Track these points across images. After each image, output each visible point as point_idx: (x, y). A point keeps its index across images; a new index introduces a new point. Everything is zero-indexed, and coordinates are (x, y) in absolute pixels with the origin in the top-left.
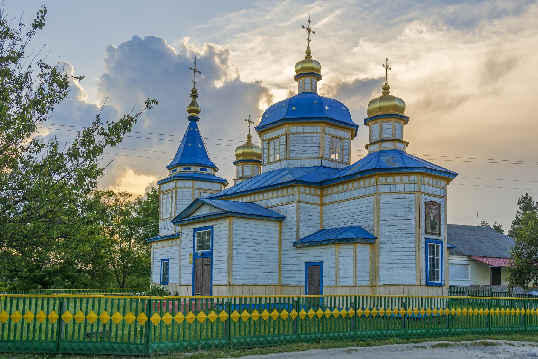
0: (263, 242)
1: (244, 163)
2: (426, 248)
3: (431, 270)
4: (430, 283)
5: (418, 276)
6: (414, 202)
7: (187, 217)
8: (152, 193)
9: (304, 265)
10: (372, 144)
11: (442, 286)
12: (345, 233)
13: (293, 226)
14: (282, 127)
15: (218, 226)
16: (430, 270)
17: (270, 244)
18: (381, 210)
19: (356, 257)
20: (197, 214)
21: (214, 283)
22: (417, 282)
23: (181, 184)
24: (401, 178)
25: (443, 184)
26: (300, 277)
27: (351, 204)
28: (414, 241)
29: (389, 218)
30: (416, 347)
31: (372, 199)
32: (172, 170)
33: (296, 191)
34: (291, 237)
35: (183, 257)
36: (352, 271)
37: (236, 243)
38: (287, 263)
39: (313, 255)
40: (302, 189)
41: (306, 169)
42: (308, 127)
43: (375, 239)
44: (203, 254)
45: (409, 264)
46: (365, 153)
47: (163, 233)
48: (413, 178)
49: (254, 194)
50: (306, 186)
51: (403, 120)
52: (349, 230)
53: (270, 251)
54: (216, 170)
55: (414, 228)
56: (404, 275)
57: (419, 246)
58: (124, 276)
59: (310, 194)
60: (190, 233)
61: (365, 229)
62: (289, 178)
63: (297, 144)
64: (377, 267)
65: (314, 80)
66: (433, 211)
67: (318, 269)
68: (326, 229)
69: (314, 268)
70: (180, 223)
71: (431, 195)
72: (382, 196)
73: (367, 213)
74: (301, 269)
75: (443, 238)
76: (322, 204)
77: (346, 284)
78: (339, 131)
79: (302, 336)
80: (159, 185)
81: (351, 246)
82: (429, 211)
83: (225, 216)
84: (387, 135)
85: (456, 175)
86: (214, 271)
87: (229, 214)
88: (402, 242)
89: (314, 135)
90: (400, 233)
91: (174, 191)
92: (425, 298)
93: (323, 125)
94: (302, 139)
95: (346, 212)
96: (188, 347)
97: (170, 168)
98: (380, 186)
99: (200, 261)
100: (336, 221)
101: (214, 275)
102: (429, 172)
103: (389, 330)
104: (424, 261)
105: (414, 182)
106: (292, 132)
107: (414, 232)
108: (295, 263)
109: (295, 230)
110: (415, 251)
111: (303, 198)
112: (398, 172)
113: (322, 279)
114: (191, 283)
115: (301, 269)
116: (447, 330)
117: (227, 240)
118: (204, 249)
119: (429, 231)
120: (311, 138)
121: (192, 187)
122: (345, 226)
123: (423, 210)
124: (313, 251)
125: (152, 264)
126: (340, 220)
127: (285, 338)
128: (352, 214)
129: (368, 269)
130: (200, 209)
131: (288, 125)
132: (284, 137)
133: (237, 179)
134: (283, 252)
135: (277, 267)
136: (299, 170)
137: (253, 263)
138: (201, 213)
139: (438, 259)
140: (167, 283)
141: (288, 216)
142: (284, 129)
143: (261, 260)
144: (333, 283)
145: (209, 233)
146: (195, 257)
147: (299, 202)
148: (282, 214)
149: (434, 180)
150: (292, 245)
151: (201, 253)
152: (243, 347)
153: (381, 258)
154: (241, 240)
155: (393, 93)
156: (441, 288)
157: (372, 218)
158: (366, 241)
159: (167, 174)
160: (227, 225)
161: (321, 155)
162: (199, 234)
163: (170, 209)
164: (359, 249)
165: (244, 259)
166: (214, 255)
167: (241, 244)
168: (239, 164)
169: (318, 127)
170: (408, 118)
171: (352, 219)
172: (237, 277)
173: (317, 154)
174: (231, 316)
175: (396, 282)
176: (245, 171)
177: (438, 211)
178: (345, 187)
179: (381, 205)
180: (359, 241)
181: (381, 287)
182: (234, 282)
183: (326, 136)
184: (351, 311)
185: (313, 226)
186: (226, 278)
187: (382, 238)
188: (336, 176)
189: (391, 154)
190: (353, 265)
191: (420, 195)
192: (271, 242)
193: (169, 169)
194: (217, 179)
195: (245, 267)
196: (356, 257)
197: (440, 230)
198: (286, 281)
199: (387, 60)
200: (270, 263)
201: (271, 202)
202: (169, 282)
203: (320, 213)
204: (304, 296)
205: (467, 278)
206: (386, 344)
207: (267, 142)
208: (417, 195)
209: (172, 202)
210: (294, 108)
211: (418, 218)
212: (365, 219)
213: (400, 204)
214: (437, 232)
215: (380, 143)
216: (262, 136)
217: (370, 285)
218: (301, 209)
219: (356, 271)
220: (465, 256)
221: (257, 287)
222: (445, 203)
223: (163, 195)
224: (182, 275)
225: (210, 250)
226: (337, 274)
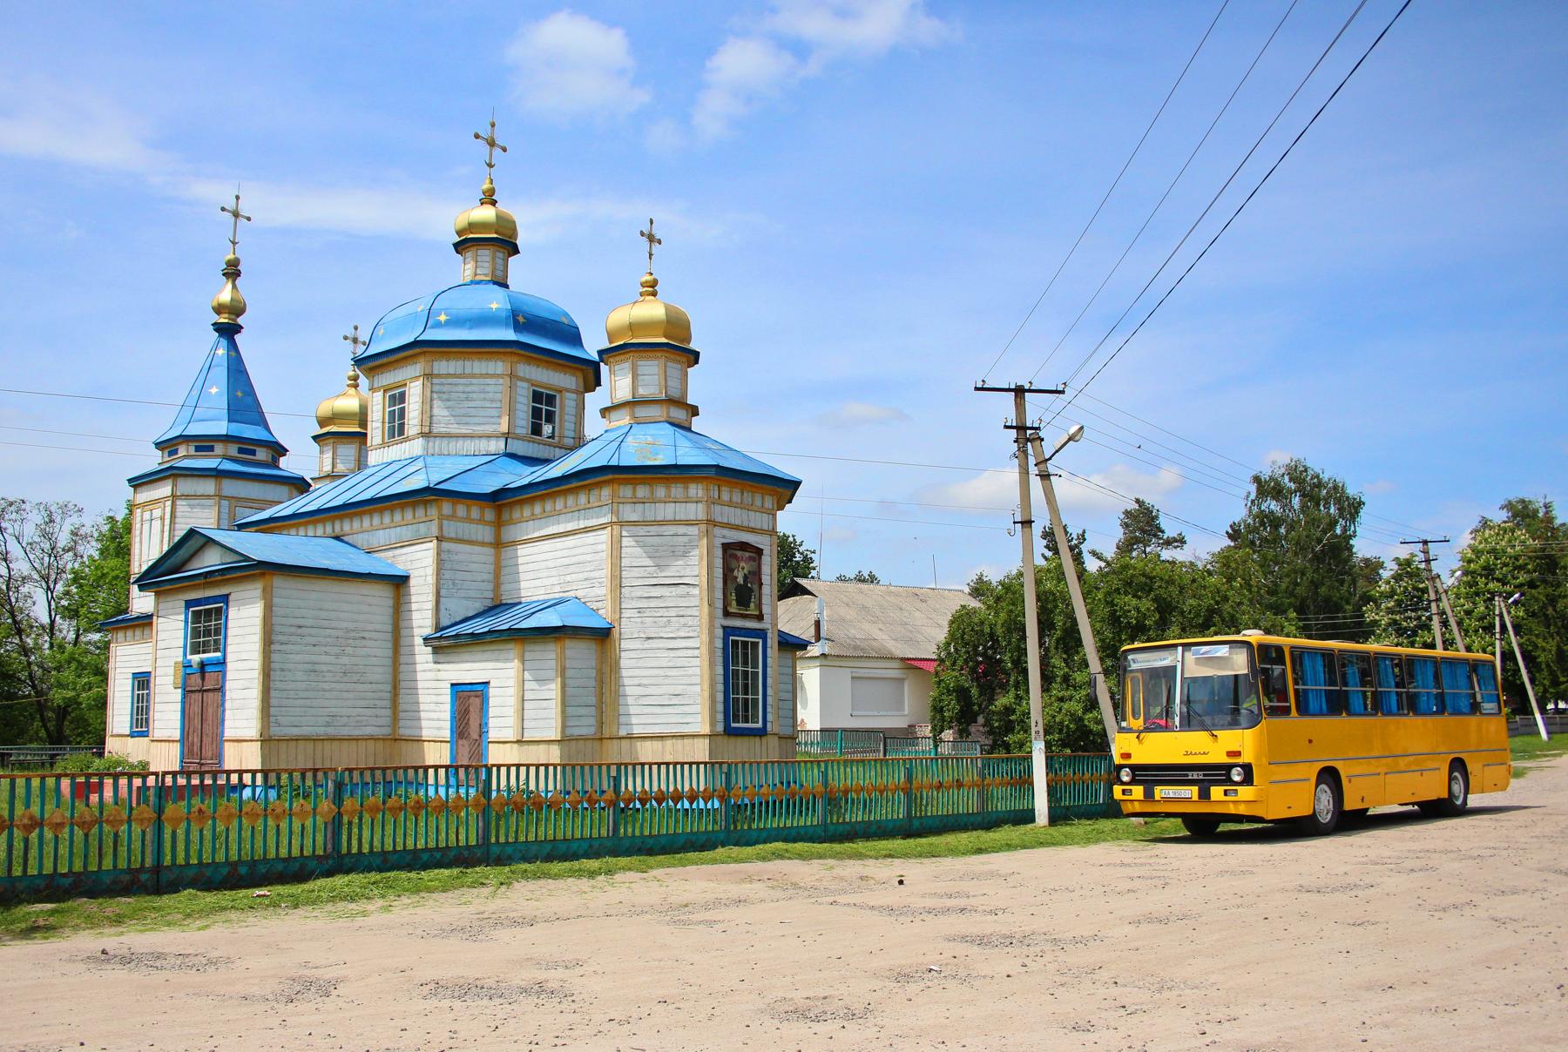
0: (352, 634)
1: (335, 440)
3: (738, 699)
4: (735, 728)
17: (370, 639)
26: (438, 720)
44: (203, 665)
53: (369, 656)
64: (613, 694)
66: (742, 564)
68: (506, 604)
75: (769, 626)
82: (734, 564)
86: (228, 705)
89: (489, 381)
94: (461, 388)
98: (621, 505)
101: (228, 714)
105: (695, 499)
106: (435, 372)
118: (209, 652)
119: (733, 609)
120: (482, 387)
137: (326, 686)
141: (413, 574)
143: (345, 679)
145: (219, 610)
154: (293, 630)
156: (764, 739)
159: (153, 460)
165: (300, 676)
166: (230, 666)
167: (293, 639)
169: (500, 364)
172: (282, 720)
183: (519, 383)
191: (710, 527)
193: (162, 450)
197: (759, 606)
200: (370, 686)
209: (163, 531)
214: (753, 611)
221: (336, 744)
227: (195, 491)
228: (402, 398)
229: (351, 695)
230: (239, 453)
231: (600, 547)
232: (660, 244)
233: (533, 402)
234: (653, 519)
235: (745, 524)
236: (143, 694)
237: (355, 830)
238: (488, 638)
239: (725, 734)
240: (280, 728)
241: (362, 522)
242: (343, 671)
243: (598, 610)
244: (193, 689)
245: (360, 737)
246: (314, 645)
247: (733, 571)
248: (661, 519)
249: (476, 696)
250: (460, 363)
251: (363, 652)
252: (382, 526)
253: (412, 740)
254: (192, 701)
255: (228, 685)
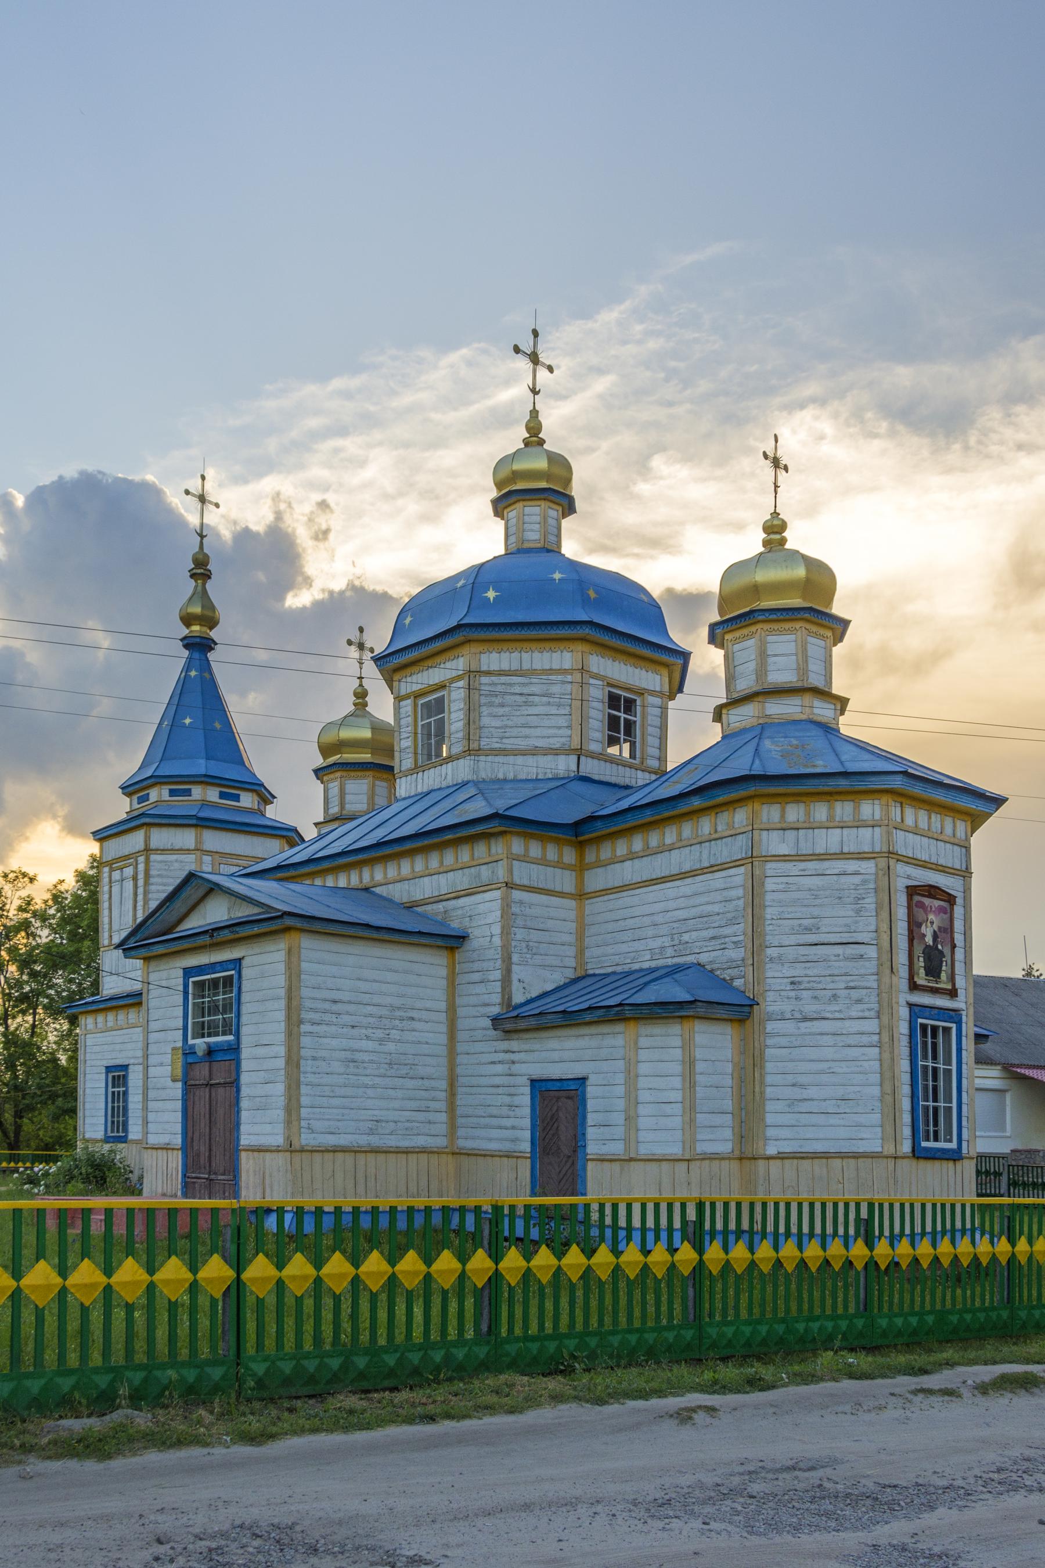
0: (398, 1013)
1: (344, 774)
2: (910, 1036)
4: (926, 1149)
5: (889, 1129)
6: (872, 886)
7: (164, 934)
8: (91, 873)
9: (527, 1090)
10: (734, 702)
11: (961, 1158)
12: (653, 987)
13: (491, 963)
14: (456, 652)
15: (256, 959)
16: (925, 1068)
17: (420, 1020)
18: (769, 910)
19: (690, 1063)
20: (194, 923)
21: (244, 1141)
22: (886, 1148)
23: (160, 837)
24: (831, 809)
25: (961, 832)
26: (513, 1128)
27: (671, 893)
28: (873, 1014)
29: (793, 939)
30: (922, 1391)
31: (739, 875)
32: (135, 797)
33: (500, 851)
34: (486, 998)
35: (152, 1060)
36: (677, 1109)
37: (311, 1015)
38: (474, 1081)
39: (555, 1055)
40: (517, 845)
41: (530, 785)
42: (536, 655)
43: (751, 1006)
45: (858, 1088)
46: (714, 734)
47: (111, 986)
48: (870, 809)
49: (371, 862)
50: (532, 836)
51: (832, 629)
52: (667, 975)
53: (419, 1042)
54: (266, 797)
55: (874, 970)
56: (842, 1122)
57: (891, 1029)
58: (18, 1115)
59: (543, 862)
60: (172, 983)
61: (718, 973)
62: (478, 808)
63: (502, 705)
64: (758, 1098)
65: (553, 513)
66: (931, 917)
67: (570, 1102)
68: (594, 975)
69: (558, 1098)
70: (143, 952)
71: (924, 865)
72: (769, 865)
73: (723, 923)
74: (517, 1100)
75: (962, 1006)
76: (581, 896)
77: (659, 1150)
78: (631, 669)
79: (512, 1349)
80: (101, 840)
81: (675, 1028)
82: (920, 914)
83: (274, 928)
84: (781, 674)
85: (998, 801)
86: (244, 1104)
87: (288, 922)
88: (837, 1015)
90: (831, 986)
91: (141, 859)
92: (934, 1205)
93: (580, 647)
94: (517, 689)
95: (659, 919)
96: (77, 1395)
97: (131, 789)
98: (765, 833)
99: (201, 1072)
100: (624, 948)
101: (244, 1115)
102: (918, 790)
103: (817, 1318)
104: (906, 1078)
105: (871, 823)
106: (484, 668)
107: (875, 985)
108: (497, 1081)
109: (497, 975)
110: (880, 1045)
111: (522, 873)
112: (821, 789)
113: (584, 1134)
114: (178, 1141)
115: (517, 1100)
116: (1005, 1314)
117: (282, 1004)
118: (217, 1034)
119: (921, 979)
120: (545, 687)
121: (192, 847)
122: (653, 964)
123: (901, 912)
124: (553, 1044)
125: (80, 1077)
126: (637, 945)
127: (448, 1358)
128: (675, 925)
129: (728, 1105)
130: (201, 907)
131: (475, 648)
132: (461, 684)
133: (326, 822)
134: (460, 1048)
135: (444, 1094)
136: (509, 786)
137: (367, 1080)
138: (205, 918)
139: (948, 1072)
140: (123, 1140)
141: (474, 933)
142: (461, 660)
144: (617, 1148)
145: (228, 981)
146: (190, 1060)
147: (509, 885)
148: (455, 925)
149: (933, 816)
150: (488, 1023)
151: (204, 1046)
152: (293, 1391)
153: (769, 1067)
154: (327, 1006)
155: (795, 539)
156: (959, 1164)
157: (741, 938)
158: (721, 1012)
159: (121, 808)
160: (281, 956)
161: (576, 744)
162: (199, 985)
163: (131, 914)
164: (699, 1039)
165: (337, 1067)
166: (245, 1053)
167: (327, 1017)
168: (332, 776)
169: (567, 655)
170: (846, 623)
171: (676, 942)
172: (317, 1125)
173: (563, 740)
174: (245, 1276)
175: (819, 1147)
176: (348, 798)
177: (946, 916)
178: (654, 839)
179: (769, 897)
180: (701, 1010)
181: (772, 1162)
182: (307, 1139)
183: (592, 681)
184: (686, 1254)
185: (555, 963)
186: (280, 1128)
187: (772, 1003)
188: (625, 804)
189: (797, 734)
190: (683, 1089)
191: (892, 862)
192: (424, 1015)
193: (129, 795)
194: (269, 823)
195: (342, 1091)
196: (690, 1063)
197: (952, 978)
198: (473, 1138)
199: (776, 441)
200: (421, 1082)
201: (425, 888)
202: (131, 1137)
203: (574, 925)
204: (524, 1199)
205: (1003, 1129)
206: (812, 1378)
207: (409, 702)
208: (882, 863)
209: (136, 894)
210: (491, 594)
211: (886, 938)
212: (719, 941)
213: (828, 893)
215: (760, 699)
216: (395, 684)
217: (737, 1153)
218: (515, 909)
219: (691, 1107)
220: (996, 1064)
221: (381, 1157)
222: (967, 891)
223: (112, 870)
224: (151, 1117)
225: (231, 1038)
226: (631, 1120)
227: (172, 844)
228: (439, 706)
229: (400, 1093)
230: (221, 797)
231: (733, 893)
232: (787, 472)
233: (609, 708)
234: (811, 852)
235: (934, 860)
236: (119, 1092)
237: (549, 1305)
238: (588, 1017)
239: (914, 1156)
240: (314, 1135)
241: (400, 868)
242: (389, 1062)
243: (732, 979)
244: (197, 1082)
245: (409, 1150)
246: (353, 1027)
247: (920, 925)
248: (822, 852)
249: (568, 1098)
250: (516, 655)
251: (409, 1036)
252: (427, 872)
253: (476, 1155)
254: (197, 1099)
255: (244, 1078)
